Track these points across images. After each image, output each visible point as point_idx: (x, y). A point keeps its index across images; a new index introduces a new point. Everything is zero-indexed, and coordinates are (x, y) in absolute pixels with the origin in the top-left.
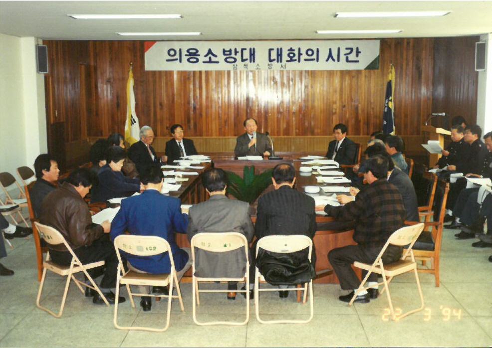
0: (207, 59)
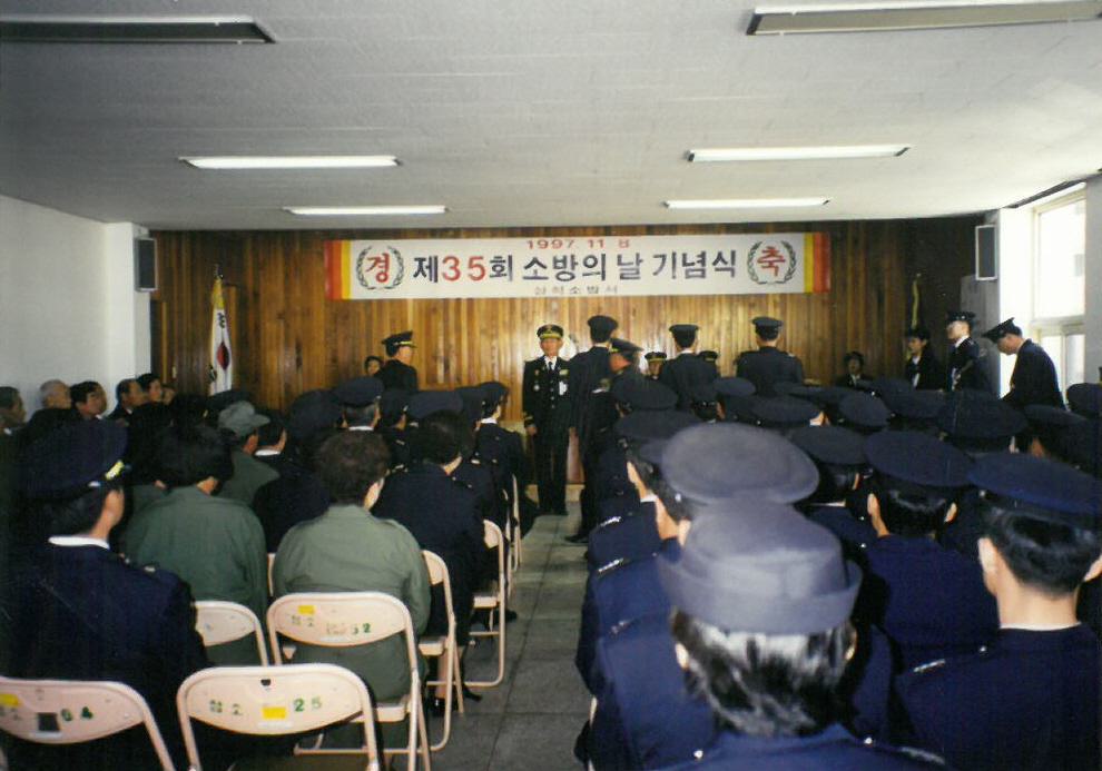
0: (530, 272)
